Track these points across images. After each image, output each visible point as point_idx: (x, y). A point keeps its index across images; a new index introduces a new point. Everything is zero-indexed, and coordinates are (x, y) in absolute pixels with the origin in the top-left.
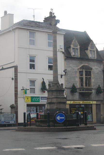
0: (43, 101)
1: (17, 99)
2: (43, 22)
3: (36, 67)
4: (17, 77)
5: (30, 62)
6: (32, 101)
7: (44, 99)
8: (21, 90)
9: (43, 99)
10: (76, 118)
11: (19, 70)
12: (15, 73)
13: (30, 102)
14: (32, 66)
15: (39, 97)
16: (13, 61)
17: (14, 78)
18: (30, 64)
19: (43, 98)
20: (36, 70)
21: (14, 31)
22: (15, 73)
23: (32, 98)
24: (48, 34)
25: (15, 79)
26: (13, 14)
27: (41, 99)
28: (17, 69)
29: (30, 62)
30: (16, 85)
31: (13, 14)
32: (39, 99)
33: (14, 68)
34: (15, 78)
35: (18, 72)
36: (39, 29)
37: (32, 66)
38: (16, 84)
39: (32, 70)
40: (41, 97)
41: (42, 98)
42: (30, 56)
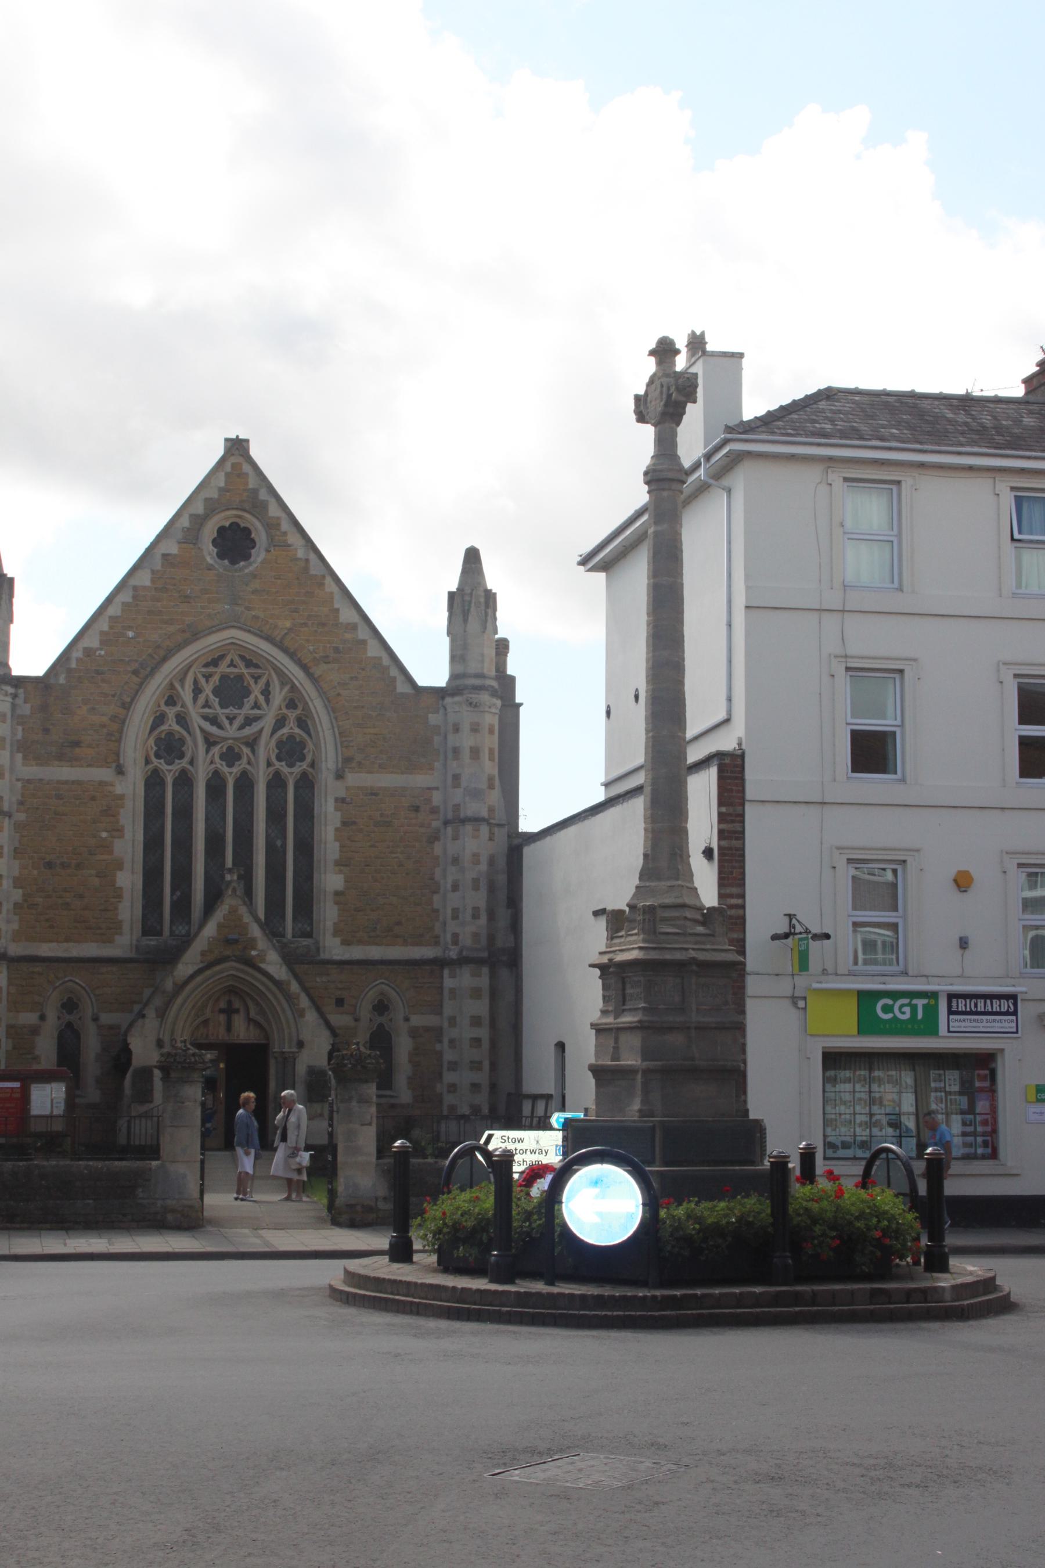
0: (960, 1023)
1: (742, 1012)
2: (1019, 391)
3: (910, 751)
4: (740, 835)
5: (1021, 722)
6: (867, 1024)
7: (996, 1008)
8: (775, 937)
9: (971, 1013)
10: (122, 1140)
11: (756, 780)
12: (724, 810)
13: (855, 1032)
14: (872, 752)
15: (934, 995)
16: (722, 715)
17: (715, 845)
18: (1025, 743)
19: (970, 1005)
20: (903, 780)
21: (725, 482)
22: (724, 810)
23: (866, 999)
24: (846, 480)
25: (720, 855)
26: (741, 355)
27: (950, 1012)
28: (742, 780)
29: (1021, 722)
30: (734, 901)
31: (741, 355)
32: (931, 1012)
33: (713, 772)
34: (724, 843)
35: (749, 794)
36: (819, 445)
37: (872, 752)
38: (731, 896)
39: (872, 785)
40: (951, 997)
41: (961, 1005)
42: (848, 669)
